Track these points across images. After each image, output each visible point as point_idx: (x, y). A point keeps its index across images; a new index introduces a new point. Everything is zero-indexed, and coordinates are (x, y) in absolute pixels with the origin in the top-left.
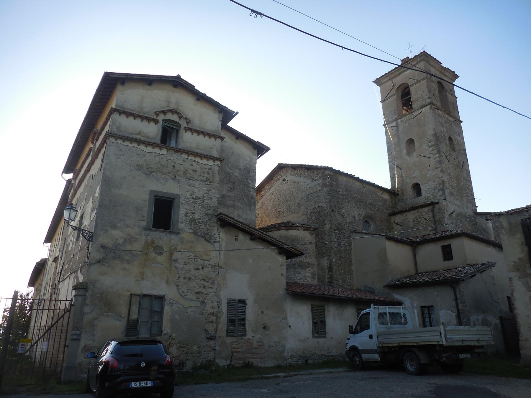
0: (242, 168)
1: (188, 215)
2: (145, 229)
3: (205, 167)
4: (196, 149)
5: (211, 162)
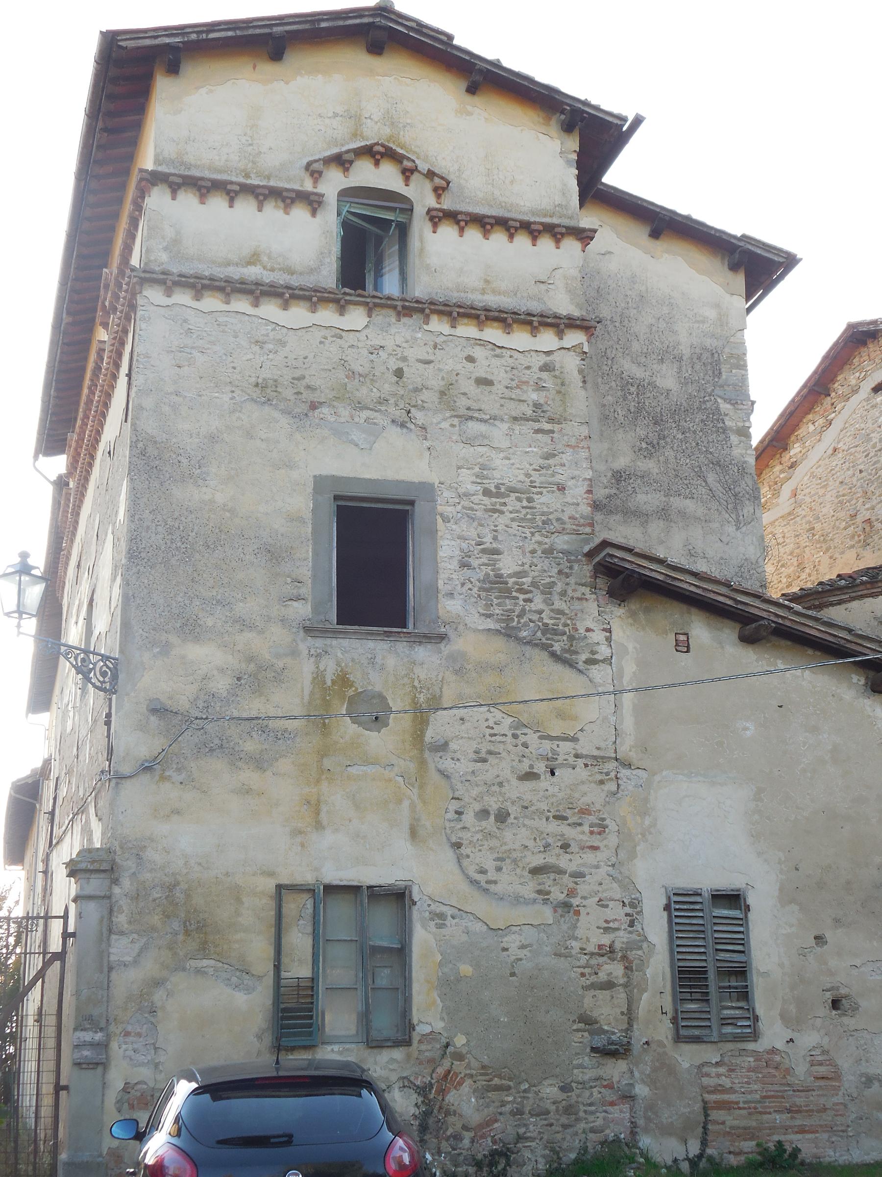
0: (686, 352)
1: (475, 563)
3: (524, 360)
4: (483, 292)
5: (547, 340)
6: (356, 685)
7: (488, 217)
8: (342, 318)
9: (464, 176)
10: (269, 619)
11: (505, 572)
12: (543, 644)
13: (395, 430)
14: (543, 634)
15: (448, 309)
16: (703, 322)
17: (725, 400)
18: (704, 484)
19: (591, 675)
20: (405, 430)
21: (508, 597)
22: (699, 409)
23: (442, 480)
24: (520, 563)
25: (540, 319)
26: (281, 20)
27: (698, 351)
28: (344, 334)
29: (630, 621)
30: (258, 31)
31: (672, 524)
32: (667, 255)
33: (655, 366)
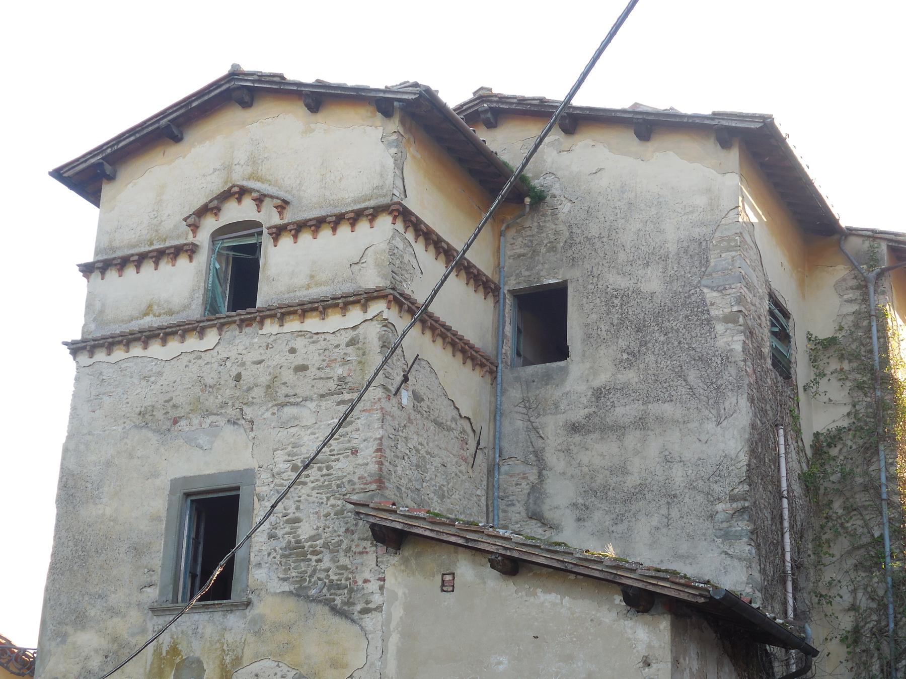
0: (672, 248)
1: (280, 533)
2: (156, 610)
3: (334, 340)
4: (308, 287)
5: (355, 315)
6: (182, 653)
7: (311, 220)
10: (129, 605)
11: (303, 537)
12: (326, 600)
13: (231, 427)
14: (329, 590)
15: (273, 312)
16: (692, 212)
17: (712, 288)
18: (684, 383)
19: (363, 625)
20: (236, 426)
21: (303, 560)
22: (683, 305)
23: (261, 464)
24: (315, 527)
25: (344, 300)
26: (164, 114)
27: (685, 244)
28: (203, 354)
29: (403, 567)
30: (150, 128)
31: (649, 432)
32: (658, 154)
33: (640, 272)
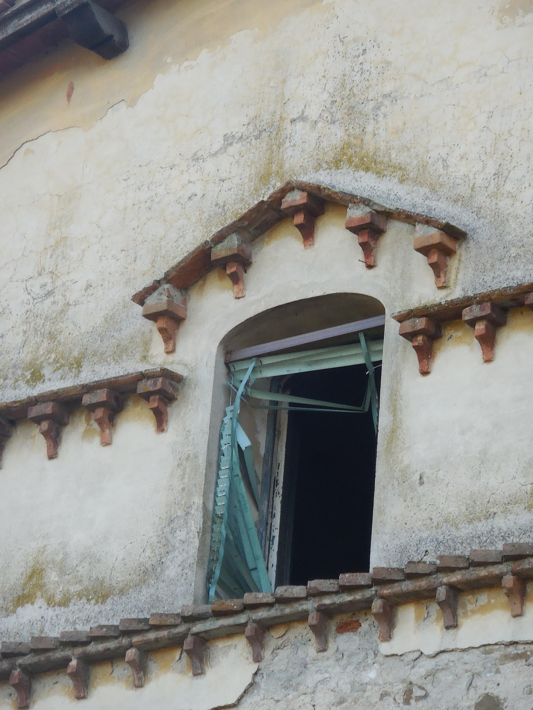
8: (200, 681)
9: (509, 187)
15: (423, 583)
